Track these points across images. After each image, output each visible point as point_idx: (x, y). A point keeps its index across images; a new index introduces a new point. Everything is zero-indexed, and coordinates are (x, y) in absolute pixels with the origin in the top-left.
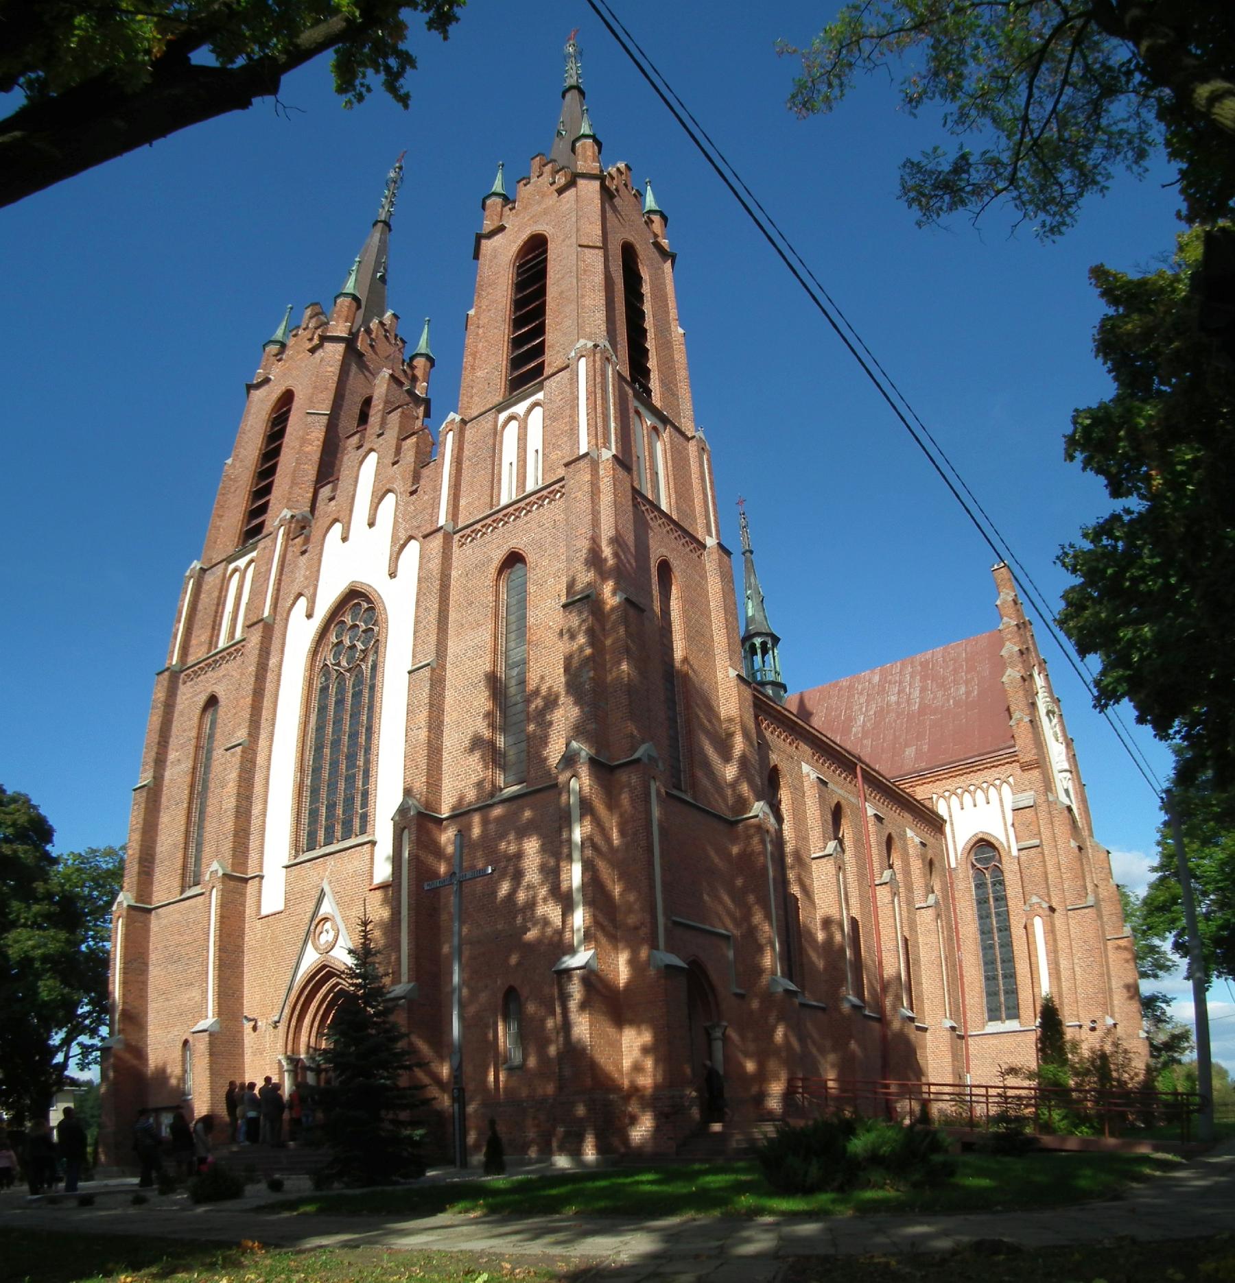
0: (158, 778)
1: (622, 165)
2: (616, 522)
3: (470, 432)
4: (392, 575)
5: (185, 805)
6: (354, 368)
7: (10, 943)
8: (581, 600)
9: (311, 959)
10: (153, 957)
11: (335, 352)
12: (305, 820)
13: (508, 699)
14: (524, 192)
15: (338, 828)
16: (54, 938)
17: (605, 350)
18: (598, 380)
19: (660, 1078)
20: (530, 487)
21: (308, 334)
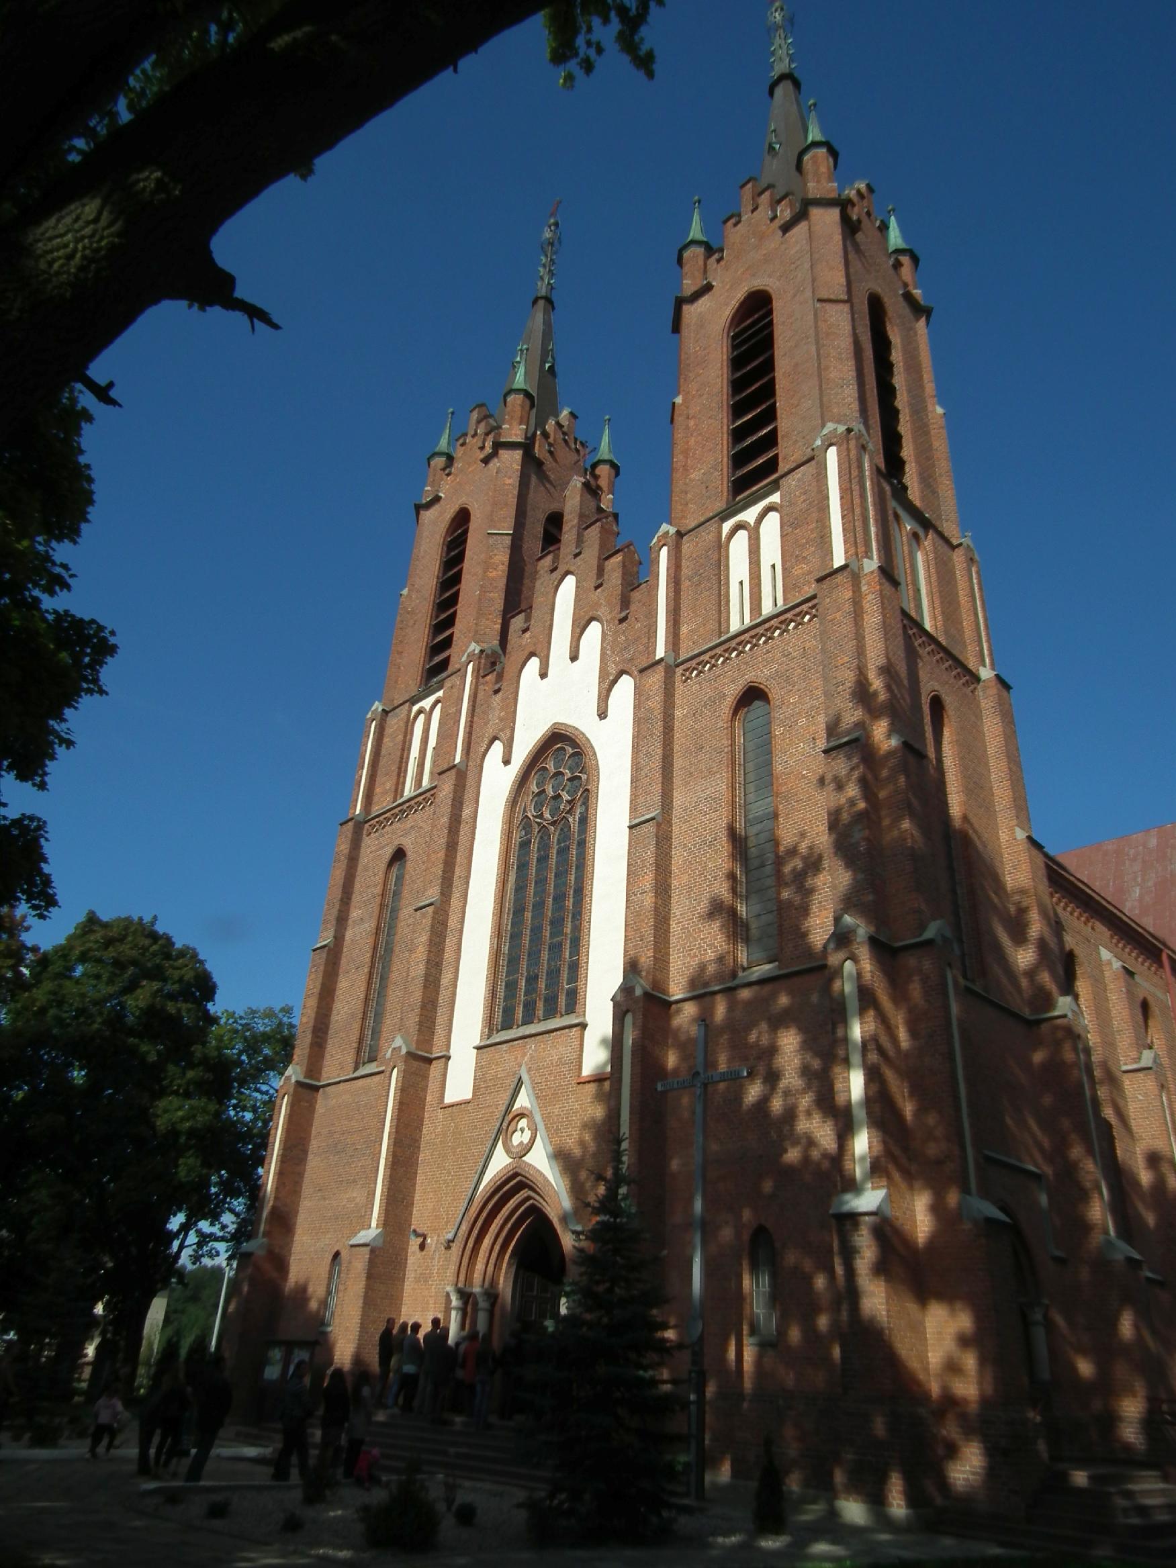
0: (339, 939)
1: (862, 186)
2: (887, 648)
3: (687, 546)
4: (603, 715)
5: (366, 970)
6: (534, 479)
7: (159, 1112)
8: (849, 744)
9: (500, 1162)
10: (314, 1145)
11: (512, 460)
12: (501, 992)
13: (756, 860)
14: (734, 235)
15: (540, 1005)
16: (204, 1111)
17: (859, 437)
18: (855, 473)
19: (989, 1390)
20: (767, 608)
21: (477, 442)
